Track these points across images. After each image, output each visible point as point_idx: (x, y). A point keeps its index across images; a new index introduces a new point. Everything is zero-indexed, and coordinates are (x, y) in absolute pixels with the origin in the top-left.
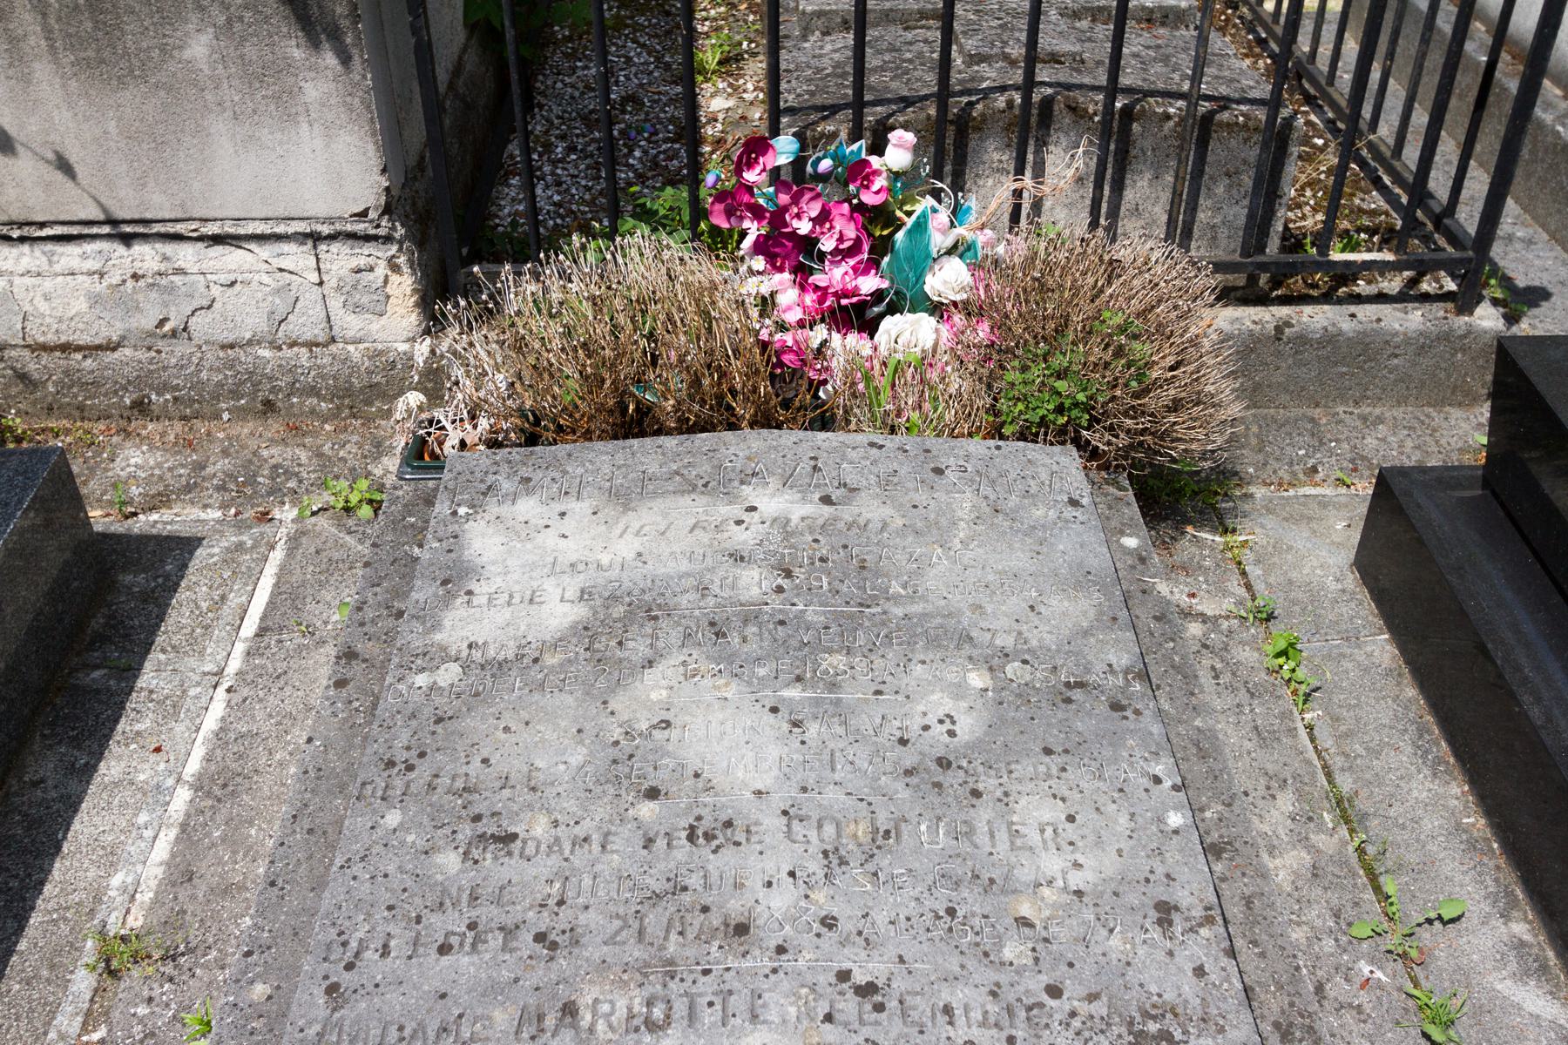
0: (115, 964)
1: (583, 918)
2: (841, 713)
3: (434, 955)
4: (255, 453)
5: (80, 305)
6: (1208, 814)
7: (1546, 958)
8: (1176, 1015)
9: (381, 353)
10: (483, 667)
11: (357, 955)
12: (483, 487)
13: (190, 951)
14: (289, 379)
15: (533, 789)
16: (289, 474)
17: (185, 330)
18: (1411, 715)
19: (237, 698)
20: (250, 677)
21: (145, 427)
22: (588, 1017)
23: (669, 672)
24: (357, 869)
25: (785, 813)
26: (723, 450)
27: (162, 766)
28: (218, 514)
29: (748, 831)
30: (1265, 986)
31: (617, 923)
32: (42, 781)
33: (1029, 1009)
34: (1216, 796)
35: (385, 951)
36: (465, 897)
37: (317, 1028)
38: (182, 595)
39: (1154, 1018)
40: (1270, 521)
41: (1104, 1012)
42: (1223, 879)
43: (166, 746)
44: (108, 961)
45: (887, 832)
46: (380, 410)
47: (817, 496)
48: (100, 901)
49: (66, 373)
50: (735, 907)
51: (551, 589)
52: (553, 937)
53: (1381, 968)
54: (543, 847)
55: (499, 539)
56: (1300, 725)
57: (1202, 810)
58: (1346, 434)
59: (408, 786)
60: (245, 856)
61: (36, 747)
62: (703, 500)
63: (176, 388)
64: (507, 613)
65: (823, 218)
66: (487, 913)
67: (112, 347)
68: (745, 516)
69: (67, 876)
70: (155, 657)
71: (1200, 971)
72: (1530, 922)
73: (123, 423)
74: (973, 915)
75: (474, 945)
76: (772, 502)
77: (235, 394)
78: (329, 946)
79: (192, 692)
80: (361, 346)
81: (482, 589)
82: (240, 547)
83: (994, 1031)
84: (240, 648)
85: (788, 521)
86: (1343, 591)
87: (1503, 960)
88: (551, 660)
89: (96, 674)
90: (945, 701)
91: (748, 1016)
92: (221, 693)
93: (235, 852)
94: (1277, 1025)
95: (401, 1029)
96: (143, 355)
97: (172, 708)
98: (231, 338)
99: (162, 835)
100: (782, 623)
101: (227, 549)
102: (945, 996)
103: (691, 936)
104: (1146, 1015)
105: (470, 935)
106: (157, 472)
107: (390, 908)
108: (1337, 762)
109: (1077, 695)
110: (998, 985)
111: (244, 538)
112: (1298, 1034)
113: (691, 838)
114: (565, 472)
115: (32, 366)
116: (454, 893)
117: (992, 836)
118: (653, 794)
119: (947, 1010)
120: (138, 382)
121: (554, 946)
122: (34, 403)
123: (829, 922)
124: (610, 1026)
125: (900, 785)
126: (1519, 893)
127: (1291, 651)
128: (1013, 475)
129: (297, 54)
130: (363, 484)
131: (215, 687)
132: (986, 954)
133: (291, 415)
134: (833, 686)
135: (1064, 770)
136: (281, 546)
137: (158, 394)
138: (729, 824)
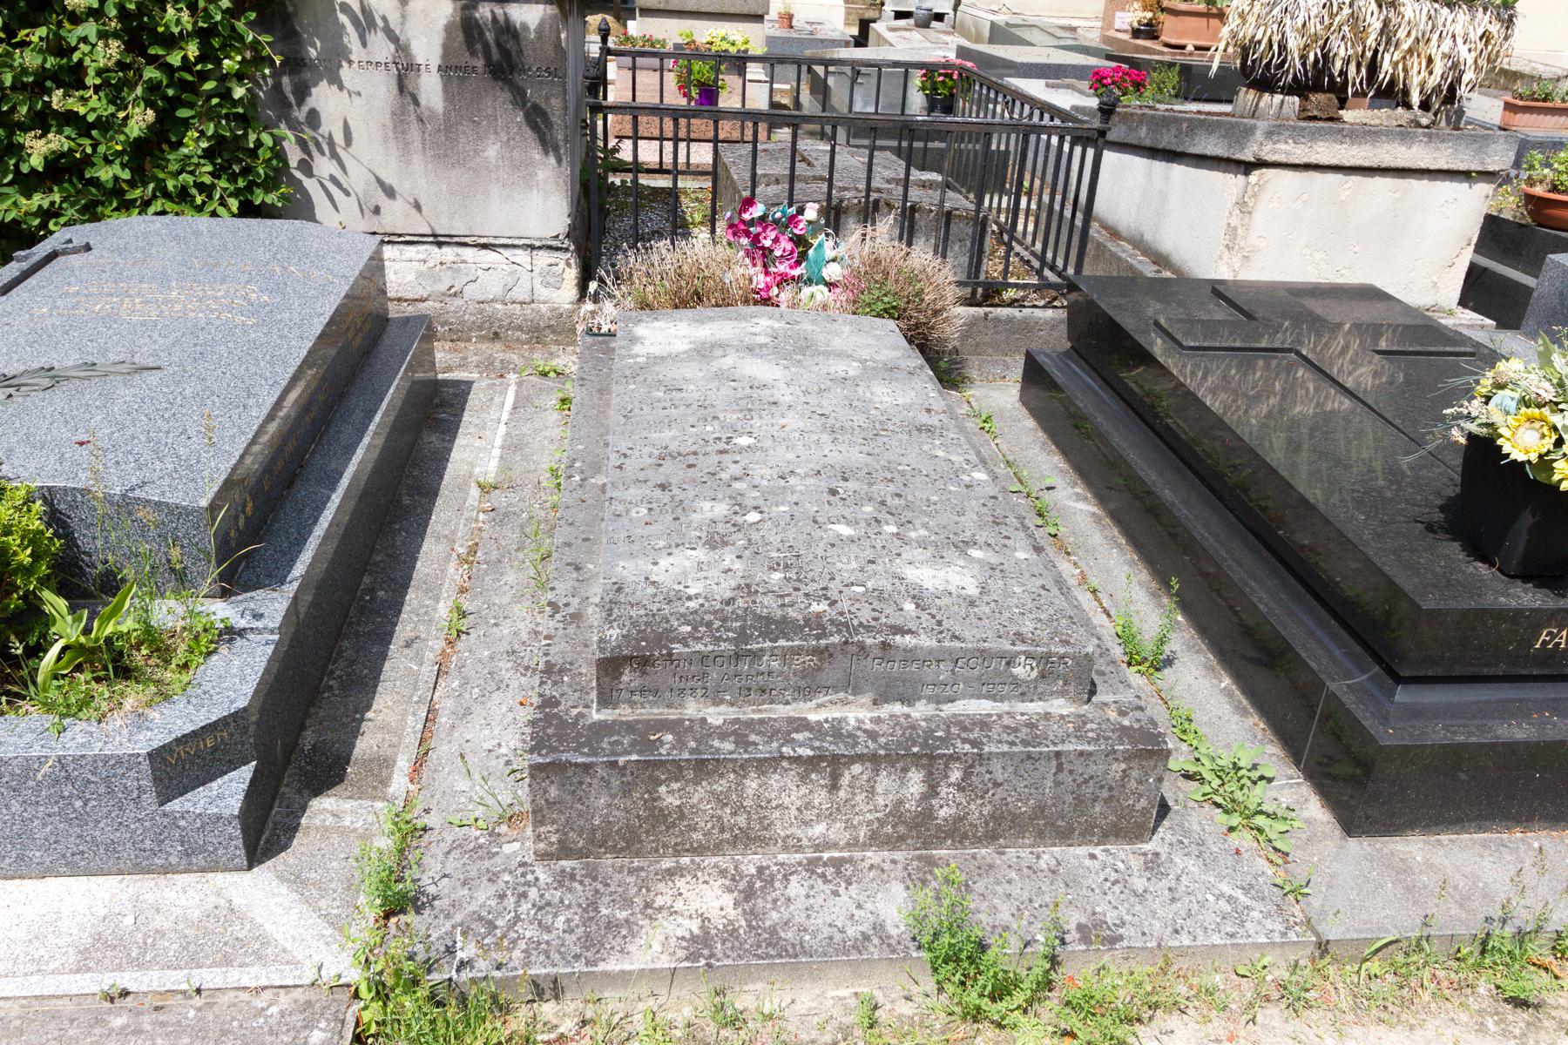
5: (411, 277)
65: (776, 240)
67: (422, 300)
77: (480, 328)
96: (438, 305)
98: (482, 298)
129: (537, 157)
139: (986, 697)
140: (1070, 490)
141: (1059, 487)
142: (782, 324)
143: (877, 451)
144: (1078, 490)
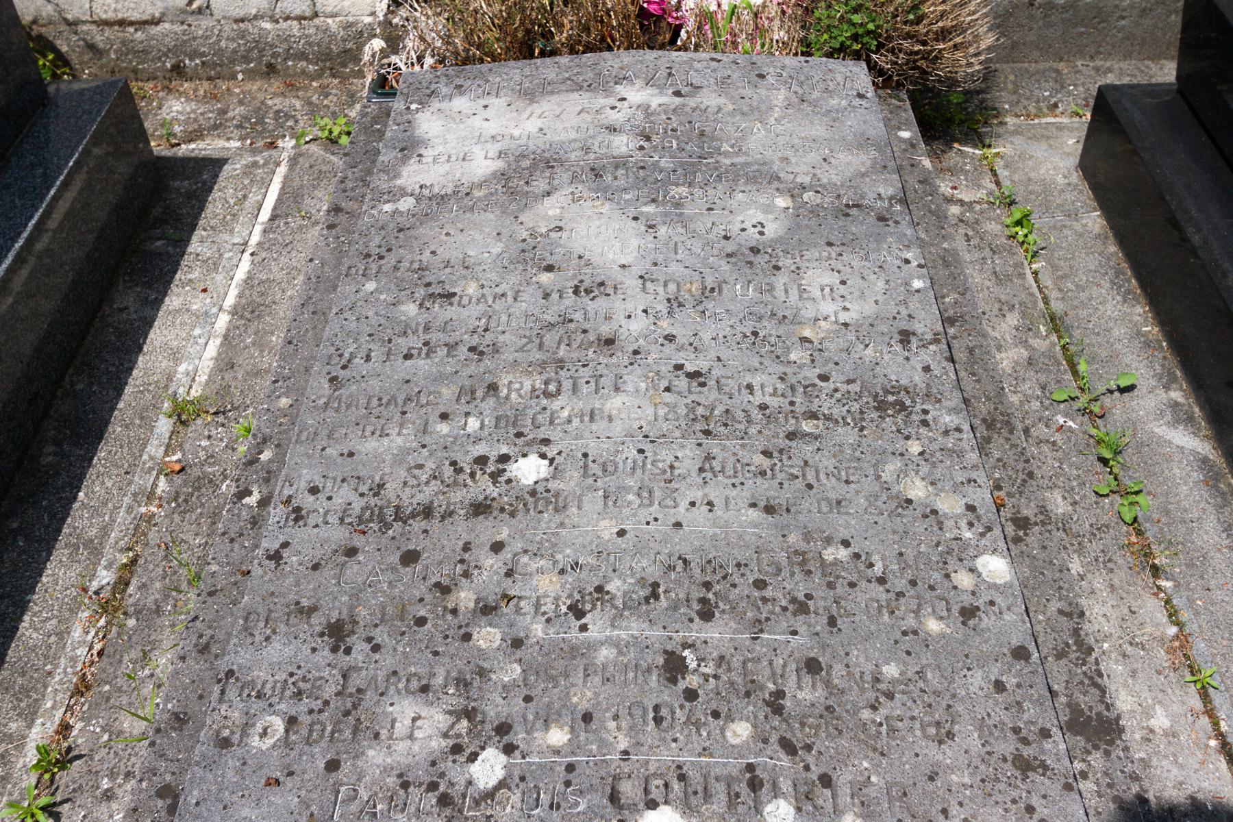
0: (184, 417)
1: (501, 338)
2: (683, 221)
3: (401, 360)
4: (262, 103)
6: (947, 300)
7: (1193, 413)
8: (908, 392)
9: (351, 25)
10: (430, 199)
11: (349, 361)
12: (428, 92)
13: (234, 409)
14: (285, 46)
15: (467, 268)
16: (288, 117)
17: (208, 7)
18: (1111, 264)
19: (258, 259)
20: (266, 246)
21: (182, 85)
22: (505, 391)
23: (562, 199)
24: (347, 314)
25: (641, 277)
26: (602, 63)
27: (208, 300)
28: (238, 144)
29: (615, 288)
30: (978, 399)
31: (524, 341)
32: (126, 308)
33: (806, 387)
35: (368, 358)
36: (421, 329)
37: (325, 400)
38: (216, 194)
39: (893, 394)
40: (1018, 140)
41: (858, 389)
42: (955, 338)
43: (210, 288)
44: (179, 416)
45: (713, 290)
46: (352, 71)
47: (670, 91)
48: (172, 381)
49: (124, 43)
50: (605, 330)
51: (478, 152)
52: (481, 348)
53: (1072, 420)
54: (474, 300)
55: (440, 123)
56: (1028, 272)
57: (943, 297)
58: (1082, 80)
59: (380, 267)
60: (269, 353)
61: (120, 288)
62: (588, 94)
63: (203, 55)
64: (447, 167)
66: (434, 337)
67: (155, 22)
68: (618, 104)
69: (149, 365)
70: (199, 233)
71: (927, 369)
72: (1184, 391)
73: (166, 83)
74: (770, 335)
75: (428, 355)
76: (636, 94)
77: (246, 59)
78: (330, 357)
79: (227, 255)
80: (337, 19)
81: (428, 153)
82: (255, 164)
83: (781, 399)
84: (258, 229)
85: (649, 106)
86: (1069, 184)
88: (477, 194)
89: (159, 243)
90: (758, 215)
91: (612, 388)
93: (262, 351)
94: (984, 420)
95: (380, 399)
96: (178, 28)
97: (213, 265)
98: (240, 13)
99: (211, 342)
100: (643, 168)
101: (246, 166)
102: (748, 379)
103: (574, 345)
104: (887, 392)
105: (425, 349)
106: (192, 116)
107: (370, 335)
108: (1053, 295)
109: (854, 212)
110: (785, 374)
111: (258, 158)
112: (999, 425)
113: (576, 291)
114: (487, 81)
115: (98, 38)
116: (413, 326)
117: (786, 291)
118: (549, 268)
119: (750, 387)
120: (176, 50)
121: (482, 353)
122: (101, 68)
123: (670, 338)
124: (520, 396)
125: (723, 263)
126: (1178, 373)
127: (1025, 222)
128: (817, 78)
130: (342, 121)
131: (242, 252)
132: (778, 357)
133: (287, 75)
134: (678, 205)
135: (841, 255)
136: (284, 163)
137: (191, 60)
138: (602, 284)
140: (1162, 395)
142: (668, 99)
143: (782, 498)
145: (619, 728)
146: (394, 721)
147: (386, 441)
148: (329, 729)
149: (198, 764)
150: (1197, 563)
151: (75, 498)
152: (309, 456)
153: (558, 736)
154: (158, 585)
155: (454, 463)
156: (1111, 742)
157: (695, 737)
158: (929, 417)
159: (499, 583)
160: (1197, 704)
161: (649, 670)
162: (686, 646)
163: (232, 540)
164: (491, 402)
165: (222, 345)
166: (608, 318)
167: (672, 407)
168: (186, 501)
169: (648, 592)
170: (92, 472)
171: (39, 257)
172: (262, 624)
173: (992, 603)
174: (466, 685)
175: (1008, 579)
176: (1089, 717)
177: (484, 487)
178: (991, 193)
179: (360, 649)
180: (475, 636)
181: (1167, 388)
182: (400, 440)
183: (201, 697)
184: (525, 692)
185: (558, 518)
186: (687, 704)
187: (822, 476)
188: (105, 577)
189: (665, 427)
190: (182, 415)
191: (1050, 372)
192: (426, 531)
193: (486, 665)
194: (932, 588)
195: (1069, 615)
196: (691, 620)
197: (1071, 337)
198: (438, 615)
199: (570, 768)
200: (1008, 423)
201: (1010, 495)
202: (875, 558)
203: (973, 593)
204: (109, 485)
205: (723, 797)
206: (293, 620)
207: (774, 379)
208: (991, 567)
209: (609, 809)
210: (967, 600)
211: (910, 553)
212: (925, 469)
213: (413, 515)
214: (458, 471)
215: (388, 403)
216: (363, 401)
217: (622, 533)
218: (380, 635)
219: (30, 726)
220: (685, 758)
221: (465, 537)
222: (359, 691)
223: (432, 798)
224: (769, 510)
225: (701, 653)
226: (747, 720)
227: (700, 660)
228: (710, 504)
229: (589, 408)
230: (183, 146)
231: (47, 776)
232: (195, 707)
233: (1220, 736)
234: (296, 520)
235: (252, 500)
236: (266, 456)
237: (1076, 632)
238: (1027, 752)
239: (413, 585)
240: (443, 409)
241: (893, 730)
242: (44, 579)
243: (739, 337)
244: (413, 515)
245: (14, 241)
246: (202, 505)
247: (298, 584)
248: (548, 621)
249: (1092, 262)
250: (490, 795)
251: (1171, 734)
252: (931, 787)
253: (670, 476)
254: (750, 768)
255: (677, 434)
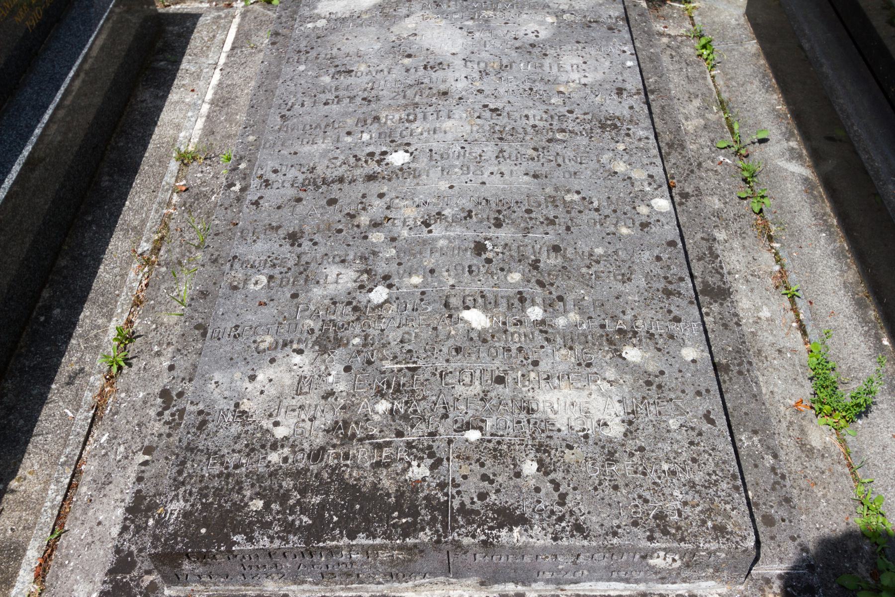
0: (186, 161)
2: (490, 30)
3: (322, 106)
13: (216, 156)
19: (224, 72)
34: (656, 74)
35: (303, 105)
36: (333, 89)
38: (195, 35)
42: (653, 100)
43: (196, 89)
45: (506, 66)
50: (443, 87)
66: (341, 93)
69: (161, 132)
71: (631, 108)
75: (338, 103)
78: (280, 105)
79: (205, 70)
82: (219, 17)
87: (783, 154)
88: (364, 17)
89: (162, 63)
92: (218, 71)
94: (667, 144)
102: (526, 112)
103: (424, 96)
104: (607, 119)
105: (336, 100)
109: (594, 25)
111: (221, 13)
113: (425, 68)
118: (409, 56)
119: (527, 117)
121: (370, 101)
123: (480, 91)
125: (513, 52)
126: (796, 132)
127: (708, 46)
134: (487, 21)
138: (441, 63)
139: (615, 580)
140: (785, 144)
141: (773, 139)
143: (544, 171)
144: (793, 144)
145: (449, 275)
146: (327, 276)
147: (315, 146)
148: (292, 280)
149: (221, 297)
150: (796, 234)
151: (124, 205)
152: (271, 155)
153: (416, 280)
154: (177, 250)
155: (355, 156)
156: (725, 299)
157: (490, 279)
158: (631, 132)
159: (383, 212)
160: (788, 305)
161: (466, 250)
162: (486, 239)
163: (226, 209)
164: (376, 125)
165: (206, 121)
166: (444, 81)
167: (482, 126)
168: (191, 206)
169: (466, 214)
170: (133, 191)
171: (86, 74)
172: (251, 235)
173: (658, 221)
174: (366, 259)
175: (668, 209)
176: (714, 288)
177: (373, 167)
178: (689, 30)
179: (306, 245)
180: (370, 237)
181: (788, 140)
182: (323, 146)
183: (215, 284)
184: (398, 261)
185: (415, 181)
186: (487, 265)
187: (567, 161)
188: (145, 246)
189: (477, 136)
190: (185, 160)
191: (717, 132)
192: (340, 189)
193: (376, 250)
194: (625, 214)
195: (707, 240)
196: (490, 228)
197: (732, 112)
198: (349, 229)
199: (423, 293)
200: (681, 145)
201: (679, 181)
202: (594, 199)
203: (648, 216)
204: (144, 197)
205: (505, 305)
206: (268, 232)
207: (541, 113)
208: (659, 204)
209: (444, 309)
210: (644, 219)
211: (614, 198)
212: (626, 157)
213: (333, 182)
214: (358, 160)
215: (316, 127)
216: (301, 127)
217: (451, 187)
218: (317, 238)
219: (110, 321)
220: (485, 288)
221: (363, 192)
222: (307, 263)
223: (349, 308)
224: (535, 176)
225: (495, 242)
226: (519, 272)
227: (494, 246)
228: (502, 174)
229: (433, 127)
230: (172, 7)
231: (122, 346)
232: (212, 288)
233: (799, 321)
234: (266, 186)
235: (237, 188)
236: (242, 166)
237: (710, 248)
238: (670, 287)
239: (334, 215)
240: (348, 130)
241: (598, 277)
242: (110, 247)
243: (521, 91)
244: (333, 182)
245: (82, 49)
246: (201, 208)
247: (269, 216)
248: (410, 229)
249: (749, 70)
250: (381, 306)
251: (770, 320)
252: (617, 301)
253: (479, 159)
254: (520, 293)
255: (484, 139)
